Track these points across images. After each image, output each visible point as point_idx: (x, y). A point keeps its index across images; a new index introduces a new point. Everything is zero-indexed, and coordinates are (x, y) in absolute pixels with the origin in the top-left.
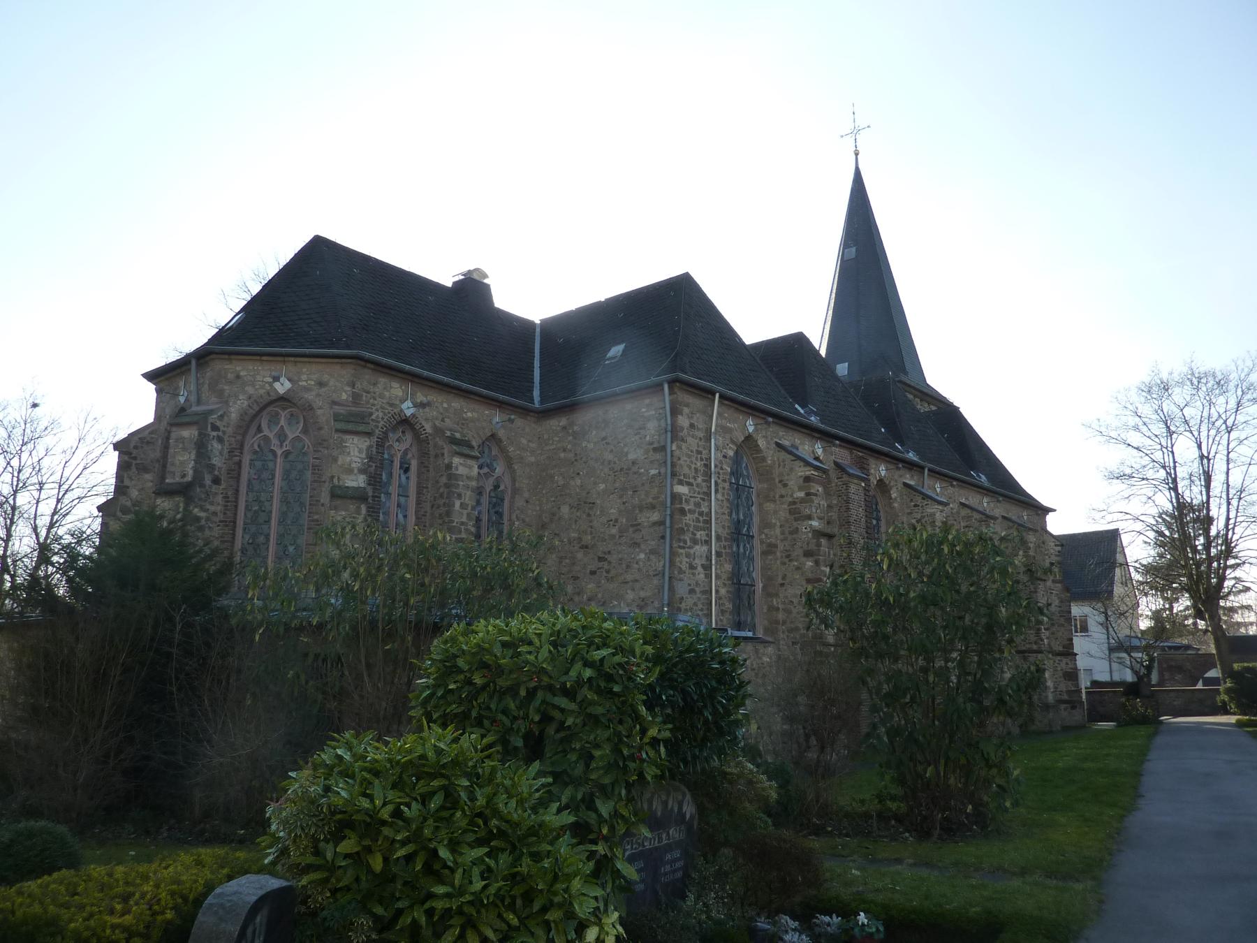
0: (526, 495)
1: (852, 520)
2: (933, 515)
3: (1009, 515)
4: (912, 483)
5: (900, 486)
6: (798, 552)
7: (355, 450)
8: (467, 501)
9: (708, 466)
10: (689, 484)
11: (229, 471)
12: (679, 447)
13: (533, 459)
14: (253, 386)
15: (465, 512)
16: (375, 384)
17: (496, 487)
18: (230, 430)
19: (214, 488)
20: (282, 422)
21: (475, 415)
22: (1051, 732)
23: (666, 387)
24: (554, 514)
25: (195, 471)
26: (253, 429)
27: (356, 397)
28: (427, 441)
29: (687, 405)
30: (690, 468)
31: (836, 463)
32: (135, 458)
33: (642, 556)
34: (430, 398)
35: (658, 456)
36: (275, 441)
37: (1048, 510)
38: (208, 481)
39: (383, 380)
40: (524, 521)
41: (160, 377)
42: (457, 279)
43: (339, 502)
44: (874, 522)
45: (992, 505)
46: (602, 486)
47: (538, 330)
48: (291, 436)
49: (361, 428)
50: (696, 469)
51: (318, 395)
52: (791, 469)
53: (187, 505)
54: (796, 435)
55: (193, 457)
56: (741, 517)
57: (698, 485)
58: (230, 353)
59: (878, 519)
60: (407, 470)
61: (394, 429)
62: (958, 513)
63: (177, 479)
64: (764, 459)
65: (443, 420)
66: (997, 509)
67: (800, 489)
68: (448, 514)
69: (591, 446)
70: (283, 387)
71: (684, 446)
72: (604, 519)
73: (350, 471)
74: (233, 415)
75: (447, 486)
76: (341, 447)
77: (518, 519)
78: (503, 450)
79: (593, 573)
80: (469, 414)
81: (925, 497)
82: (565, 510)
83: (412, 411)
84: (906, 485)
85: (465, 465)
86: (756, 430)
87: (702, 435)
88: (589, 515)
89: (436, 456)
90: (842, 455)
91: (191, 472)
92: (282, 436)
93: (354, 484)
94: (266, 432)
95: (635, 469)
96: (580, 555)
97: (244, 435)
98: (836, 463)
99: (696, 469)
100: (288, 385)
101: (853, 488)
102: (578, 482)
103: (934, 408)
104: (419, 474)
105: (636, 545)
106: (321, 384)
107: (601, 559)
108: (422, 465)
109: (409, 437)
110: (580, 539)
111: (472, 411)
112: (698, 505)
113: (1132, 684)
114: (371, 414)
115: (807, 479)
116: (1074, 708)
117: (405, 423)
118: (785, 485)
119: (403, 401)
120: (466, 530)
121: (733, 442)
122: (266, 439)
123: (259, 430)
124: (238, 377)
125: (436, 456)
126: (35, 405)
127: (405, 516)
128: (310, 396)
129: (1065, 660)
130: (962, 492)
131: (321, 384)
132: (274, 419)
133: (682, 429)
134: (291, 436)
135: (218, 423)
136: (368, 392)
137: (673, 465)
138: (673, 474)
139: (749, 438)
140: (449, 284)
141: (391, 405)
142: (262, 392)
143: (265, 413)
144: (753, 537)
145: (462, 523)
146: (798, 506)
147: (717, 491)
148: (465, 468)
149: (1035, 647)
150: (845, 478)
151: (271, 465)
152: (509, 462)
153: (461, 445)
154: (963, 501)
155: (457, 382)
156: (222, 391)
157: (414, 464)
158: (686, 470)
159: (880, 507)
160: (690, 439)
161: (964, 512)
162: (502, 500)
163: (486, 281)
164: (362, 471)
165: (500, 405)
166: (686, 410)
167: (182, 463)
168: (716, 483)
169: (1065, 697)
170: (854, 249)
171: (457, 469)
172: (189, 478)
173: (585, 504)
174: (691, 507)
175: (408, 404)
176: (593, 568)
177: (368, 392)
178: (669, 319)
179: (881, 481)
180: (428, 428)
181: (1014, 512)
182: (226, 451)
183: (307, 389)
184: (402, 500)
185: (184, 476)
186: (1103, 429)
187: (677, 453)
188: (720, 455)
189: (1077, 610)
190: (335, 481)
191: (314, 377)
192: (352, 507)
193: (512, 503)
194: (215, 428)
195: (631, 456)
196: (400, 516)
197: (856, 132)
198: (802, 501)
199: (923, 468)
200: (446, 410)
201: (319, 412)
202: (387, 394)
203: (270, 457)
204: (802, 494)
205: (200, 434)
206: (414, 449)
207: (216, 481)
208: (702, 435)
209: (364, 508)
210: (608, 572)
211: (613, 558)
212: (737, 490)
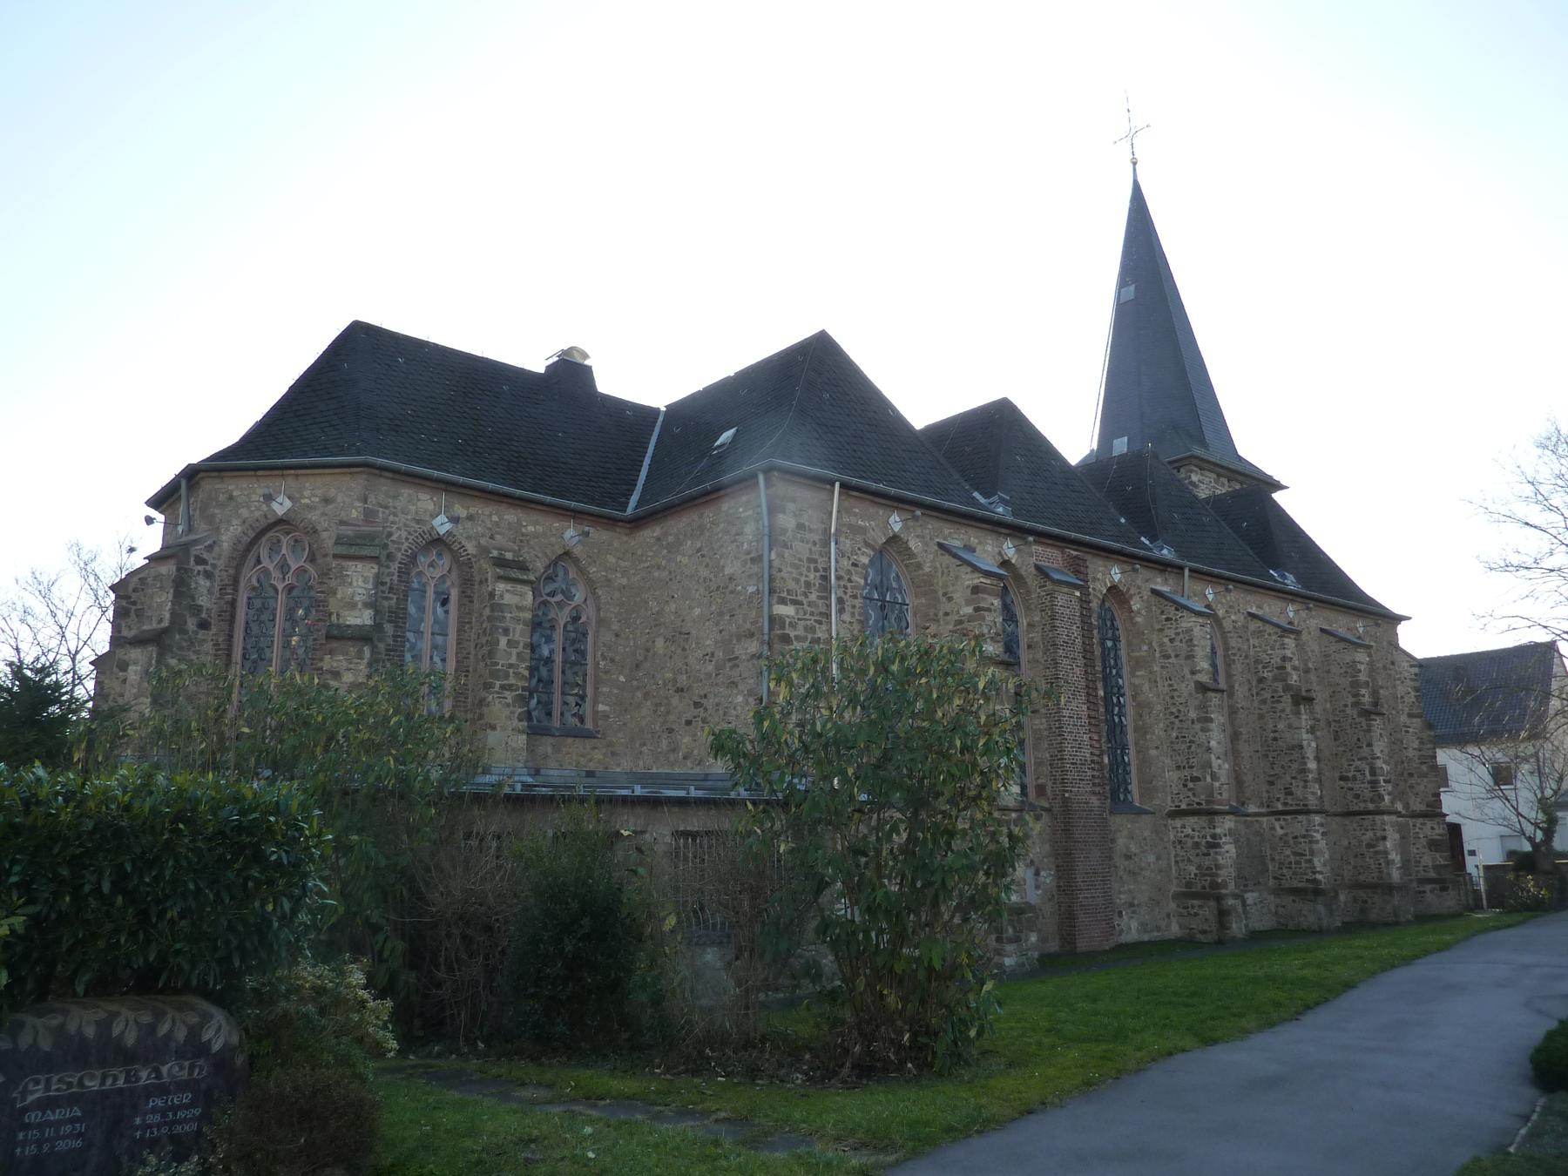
0: (616, 627)
1: (1059, 642)
2: (1190, 630)
3: (1334, 627)
4: (1165, 589)
5: (1146, 594)
7: (359, 580)
8: (517, 637)
9: (826, 578)
10: (796, 603)
11: (221, 613)
13: (624, 581)
14: (248, 507)
15: (514, 651)
16: (395, 497)
17: (576, 619)
18: (221, 563)
19: (201, 634)
20: (284, 551)
21: (540, 529)
22: (1397, 923)
23: (761, 478)
24: (648, 650)
25: (173, 614)
26: (251, 560)
27: (369, 515)
28: (469, 564)
29: (794, 500)
30: (797, 581)
31: (1038, 568)
32: (134, 603)
33: (740, 699)
35: (755, 569)
36: (276, 574)
37: (1399, 619)
38: (191, 624)
39: (406, 492)
40: (612, 660)
41: (157, 502)
42: (551, 361)
43: (335, 644)
44: (1109, 644)
45: (1303, 614)
46: (697, 611)
47: (661, 419)
48: (294, 567)
49: (366, 552)
50: (808, 584)
51: (324, 514)
52: (957, 577)
53: (161, 655)
54: (971, 531)
55: (170, 597)
57: (810, 604)
58: (256, 469)
59: (1116, 640)
60: (445, 602)
62: (1245, 627)
63: (155, 625)
64: (919, 566)
65: (492, 537)
66: (1312, 621)
67: (968, 603)
68: (491, 654)
69: (685, 560)
70: (282, 506)
71: (787, 553)
72: (700, 653)
73: (352, 606)
74: (225, 545)
75: (490, 619)
76: (343, 579)
77: (604, 658)
78: (582, 571)
79: (689, 723)
80: (531, 528)
81: (1180, 607)
82: (660, 643)
83: (448, 526)
84: (1155, 592)
85: (514, 593)
86: (905, 528)
87: (816, 538)
88: (684, 649)
89: (481, 582)
90: (1051, 557)
91: (167, 616)
92: (283, 567)
93: (358, 622)
94: (266, 563)
95: (731, 587)
96: (675, 701)
97: (238, 568)
98: (1038, 568)
99: (808, 584)
100: (288, 504)
101: (1061, 599)
102: (673, 607)
103: (1238, 487)
104: (461, 605)
105: (734, 684)
107: (697, 705)
108: (466, 596)
109: (445, 563)
110: (675, 680)
111: (536, 523)
112: (808, 629)
113: (1527, 855)
114: (390, 534)
115: (976, 590)
116: (1444, 889)
117: (437, 542)
118: (950, 599)
119: (434, 516)
120: (517, 674)
121: (867, 544)
122: (266, 571)
123: (259, 562)
124: (231, 498)
125: (481, 582)
126: (132, 550)
127: (443, 660)
128: (313, 516)
129: (1429, 824)
130: (1250, 597)
131: (327, 501)
132: (275, 548)
133: (785, 531)
134: (294, 567)
135: (205, 556)
136: (386, 507)
137: (771, 579)
138: (771, 591)
139: (894, 539)
140: (542, 370)
141: (418, 522)
142: (257, 514)
143: (264, 539)
145: (511, 666)
146: (966, 625)
147: (841, 611)
148: (516, 598)
149: (1371, 806)
150: (1049, 586)
151: (271, 602)
152: (591, 585)
153: (511, 568)
154: (1253, 610)
155: (512, 490)
156: (213, 516)
157: (454, 594)
158: (791, 585)
159: (1118, 623)
160: (797, 545)
161: (1254, 625)
162: (585, 635)
163: (587, 362)
164: (367, 605)
165: (576, 515)
166: (791, 506)
167: (160, 605)
168: (840, 601)
169: (1432, 874)
170: (1132, 288)
171: (502, 596)
172: (165, 624)
173: (679, 636)
174: (800, 632)
175: (442, 518)
176: (687, 716)
177: (386, 507)
178: (810, 391)
179: (1113, 589)
180: (471, 548)
181: (1341, 624)
182: (217, 588)
183: (309, 508)
184: (439, 639)
185: (161, 621)
186: (1488, 504)
187: (776, 564)
188: (845, 563)
189: (1444, 756)
190: (334, 618)
191: (319, 492)
192: (353, 650)
193: (596, 637)
194: (200, 561)
195: (728, 571)
196: (437, 659)
197: (1132, 135)
198: (971, 619)
199: (1181, 568)
200: (497, 524)
201: (325, 535)
202: (413, 508)
203: (272, 593)
204: (969, 610)
205: (178, 570)
206: (454, 574)
207: (204, 625)
208: (816, 538)
209: (367, 651)
210: (704, 721)
211: (709, 703)
212: (882, 608)
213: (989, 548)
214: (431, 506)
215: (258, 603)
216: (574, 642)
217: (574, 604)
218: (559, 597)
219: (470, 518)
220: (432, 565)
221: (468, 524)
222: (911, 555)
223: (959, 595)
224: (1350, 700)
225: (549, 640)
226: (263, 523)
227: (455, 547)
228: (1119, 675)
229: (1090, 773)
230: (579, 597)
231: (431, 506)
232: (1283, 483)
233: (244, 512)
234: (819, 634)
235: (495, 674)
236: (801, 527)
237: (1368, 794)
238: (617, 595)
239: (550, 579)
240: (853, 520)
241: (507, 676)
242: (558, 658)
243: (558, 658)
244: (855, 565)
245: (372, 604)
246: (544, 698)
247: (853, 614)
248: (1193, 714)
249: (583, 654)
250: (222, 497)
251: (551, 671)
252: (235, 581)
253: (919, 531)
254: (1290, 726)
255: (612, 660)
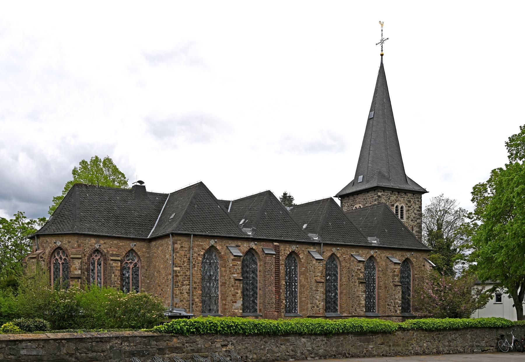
6: (231, 285)
10: (179, 267)
12: (176, 255)
18: (46, 257)
26: (53, 256)
29: (180, 240)
30: (181, 261)
34: (105, 241)
36: (59, 260)
38: (41, 273)
39: (88, 239)
50: (184, 262)
56: (212, 273)
60: (100, 265)
61: (94, 253)
64: (220, 253)
68: (110, 279)
70: (59, 244)
78: (136, 253)
82: (156, 273)
92: (61, 258)
97: (50, 259)
99: (184, 262)
100: (60, 243)
104: (104, 266)
106: (69, 242)
108: (105, 264)
117: (97, 251)
122: (57, 259)
123: (55, 257)
128: (66, 246)
131: (69, 242)
132: (58, 254)
133: (177, 249)
134: (63, 258)
138: (173, 264)
144: (218, 280)
158: (179, 262)
162: (138, 270)
164: (79, 269)
166: (179, 242)
174: (181, 274)
184: (99, 274)
194: (42, 258)
196: (99, 279)
197: (382, 42)
200: (112, 244)
213: (245, 245)
214: (94, 242)
215: (56, 267)
216: (135, 272)
217: (134, 262)
218: (130, 261)
219: (105, 243)
220: (96, 256)
221: (104, 245)
222: (218, 250)
223: (230, 261)
224: (392, 280)
225: (128, 272)
226: (55, 248)
227: (101, 251)
228: (296, 277)
229: (274, 306)
230: (136, 261)
231: (94, 242)
232: (427, 190)
233: (51, 245)
234: (187, 274)
235: (111, 284)
236: (182, 247)
237: (393, 310)
238: (146, 259)
239: (128, 256)
240: (198, 243)
241: (114, 284)
242: (131, 277)
243: (131, 277)
244: (199, 255)
245: (81, 269)
246: (127, 287)
247: (198, 268)
248: (314, 289)
249: (138, 275)
250: (45, 241)
251: (129, 280)
252: (50, 262)
253: (220, 243)
254: (357, 290)
255: (145, 277)
